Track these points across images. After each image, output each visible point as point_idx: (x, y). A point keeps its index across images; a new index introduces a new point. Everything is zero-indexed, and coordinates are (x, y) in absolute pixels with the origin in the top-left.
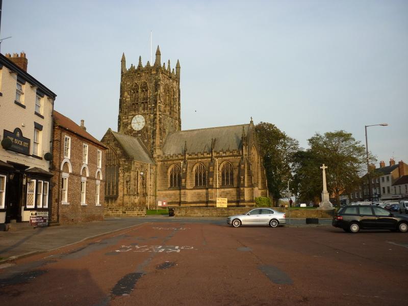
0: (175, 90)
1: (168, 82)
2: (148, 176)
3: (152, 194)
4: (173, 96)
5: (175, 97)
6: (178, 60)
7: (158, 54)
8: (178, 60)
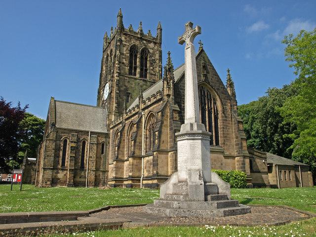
0: (151, 51)
1: (137, 43)
2: (87, 146)
5: (153, 58)
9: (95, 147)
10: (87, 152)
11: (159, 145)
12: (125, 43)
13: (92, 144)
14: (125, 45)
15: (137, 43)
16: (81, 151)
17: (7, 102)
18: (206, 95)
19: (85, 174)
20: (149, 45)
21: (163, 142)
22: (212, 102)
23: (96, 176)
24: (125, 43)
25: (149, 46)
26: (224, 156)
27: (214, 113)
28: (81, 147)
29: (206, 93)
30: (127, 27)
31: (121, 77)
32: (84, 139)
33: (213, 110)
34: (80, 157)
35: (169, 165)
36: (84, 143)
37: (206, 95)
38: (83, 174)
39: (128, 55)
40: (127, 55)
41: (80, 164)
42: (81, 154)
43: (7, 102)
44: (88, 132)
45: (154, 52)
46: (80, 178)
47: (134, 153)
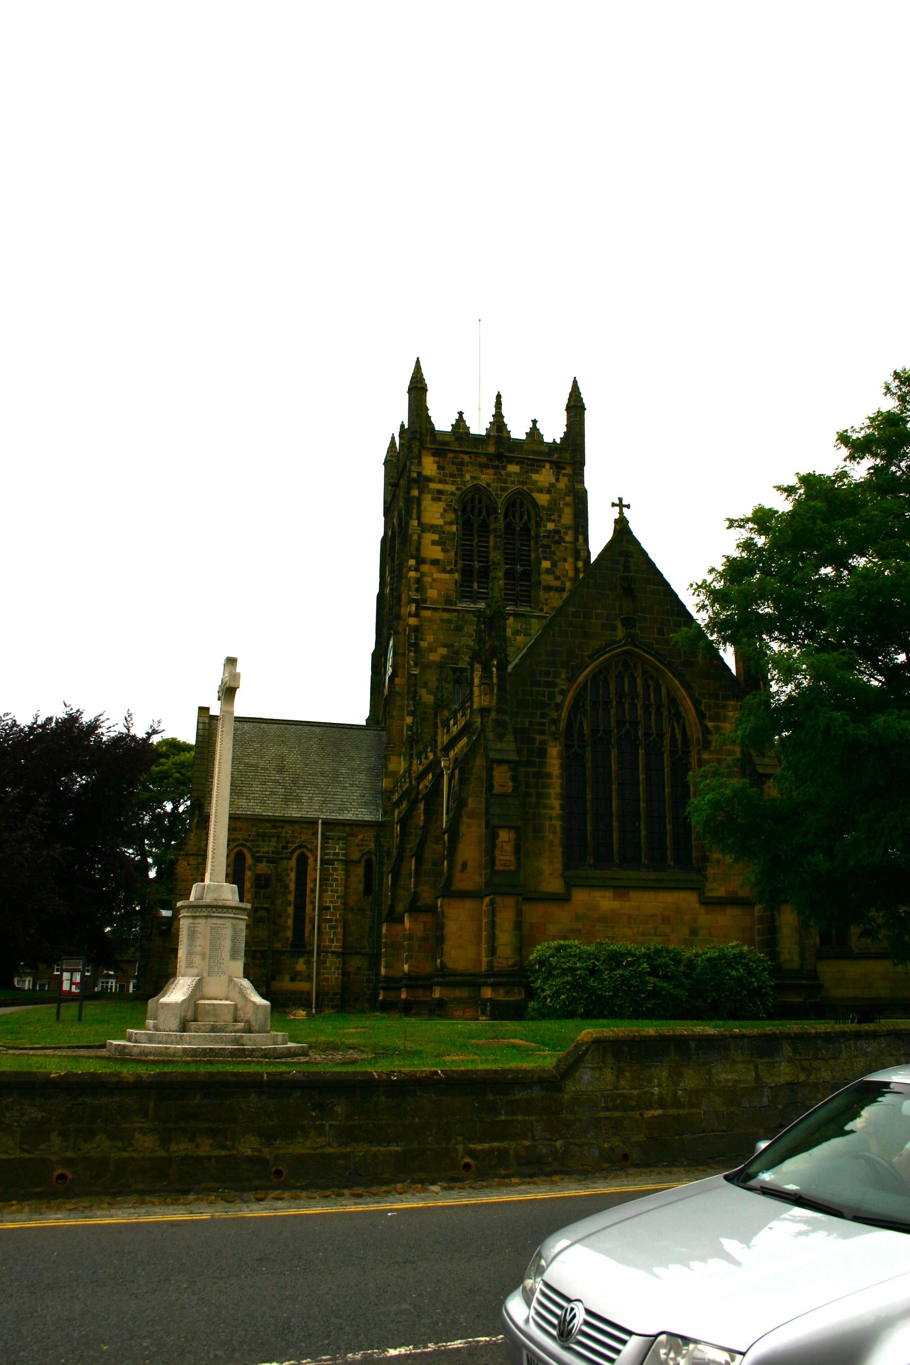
0: (543, 499)
1: (486, 478)
2: (315, 873)
3: (336, 946)
4: (538, 525)
5: (551, 526)
6: (418, 362)
7: (418, 388)
8: (418, 362)
9: (338, 874)
10: (313, 891)
11: (450, 877)
12: (440, 487)
13: (331, 862)
14: (440, 492)
15: (486, 478)
16: (292, 887)
17: (86, 719)
18: (640, 689)
19: (310, 968)
20: (535, 477)
21: (464, 865)
22: (665, 714)
23: (345, 974)
24: (440, 487)
25: (535, 483)
26: (702, 903)
27: (673, 753)
28: (293, 875)
29: (639, 681)
30: (442, 422)
31: (427, 614)
32: (301, 847)
33: (666, 742)
34: (291, 910)
35: (483, 941)
36: (303, 861)
37: (640, 689)
38: (301, 966)
39: (454, 528)
40: (447, 528)
41: (289, 934)
42: (291, 898)
43: (86, 719)
44: (313, 823)
45: (554, 502)
46: (293, 979)
47: (415, 896)
